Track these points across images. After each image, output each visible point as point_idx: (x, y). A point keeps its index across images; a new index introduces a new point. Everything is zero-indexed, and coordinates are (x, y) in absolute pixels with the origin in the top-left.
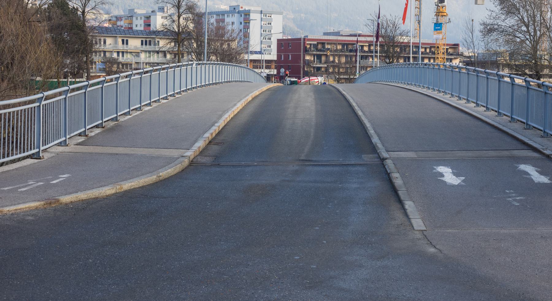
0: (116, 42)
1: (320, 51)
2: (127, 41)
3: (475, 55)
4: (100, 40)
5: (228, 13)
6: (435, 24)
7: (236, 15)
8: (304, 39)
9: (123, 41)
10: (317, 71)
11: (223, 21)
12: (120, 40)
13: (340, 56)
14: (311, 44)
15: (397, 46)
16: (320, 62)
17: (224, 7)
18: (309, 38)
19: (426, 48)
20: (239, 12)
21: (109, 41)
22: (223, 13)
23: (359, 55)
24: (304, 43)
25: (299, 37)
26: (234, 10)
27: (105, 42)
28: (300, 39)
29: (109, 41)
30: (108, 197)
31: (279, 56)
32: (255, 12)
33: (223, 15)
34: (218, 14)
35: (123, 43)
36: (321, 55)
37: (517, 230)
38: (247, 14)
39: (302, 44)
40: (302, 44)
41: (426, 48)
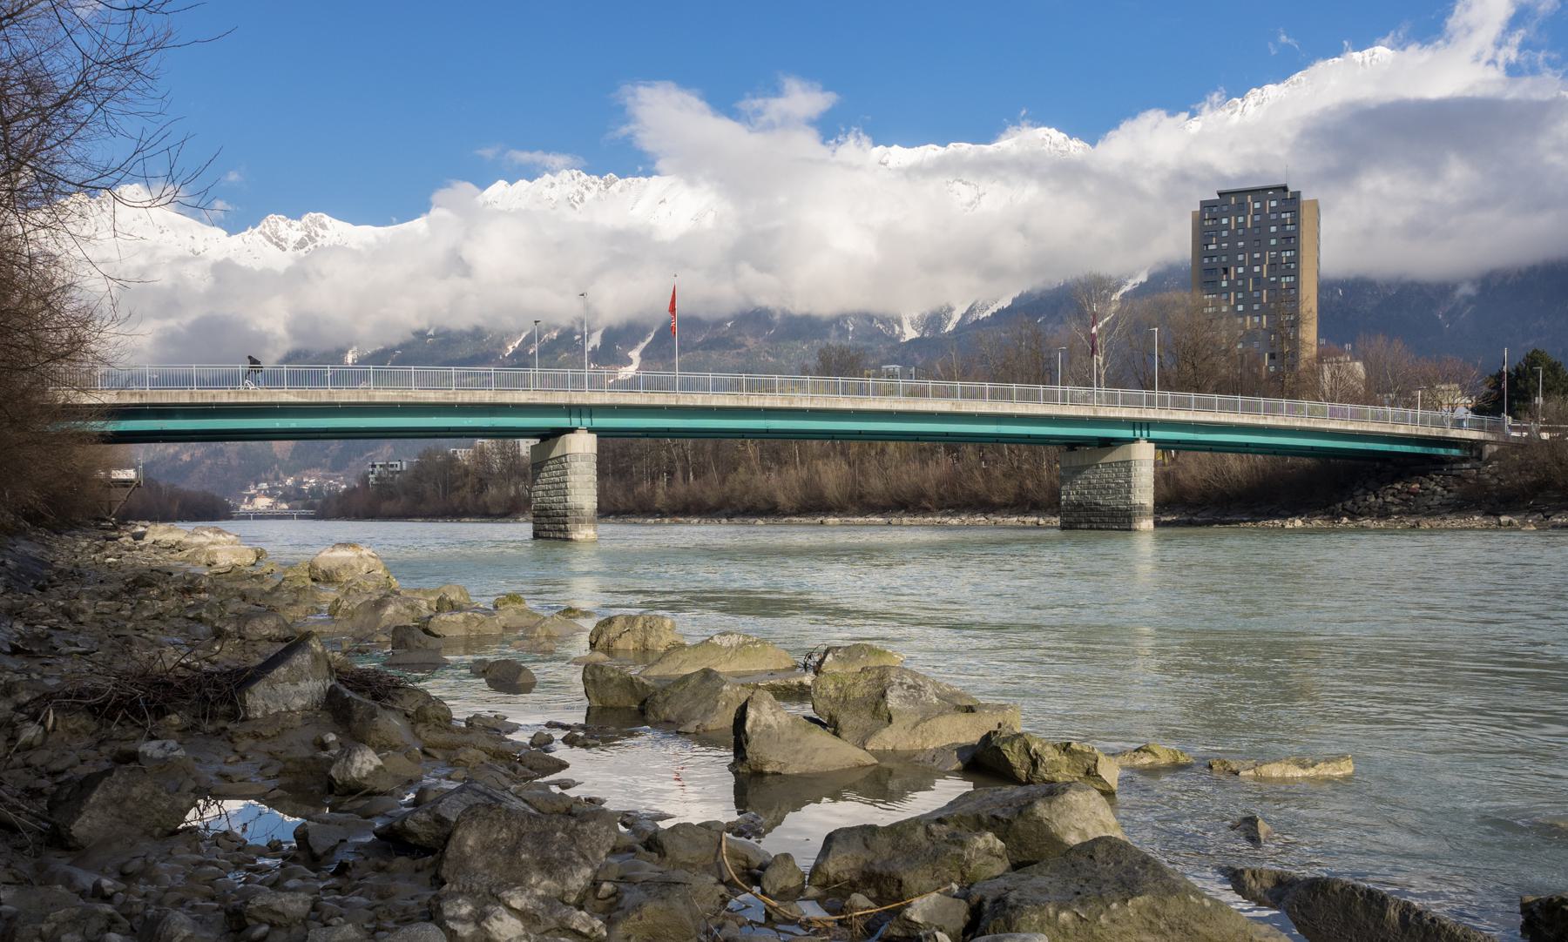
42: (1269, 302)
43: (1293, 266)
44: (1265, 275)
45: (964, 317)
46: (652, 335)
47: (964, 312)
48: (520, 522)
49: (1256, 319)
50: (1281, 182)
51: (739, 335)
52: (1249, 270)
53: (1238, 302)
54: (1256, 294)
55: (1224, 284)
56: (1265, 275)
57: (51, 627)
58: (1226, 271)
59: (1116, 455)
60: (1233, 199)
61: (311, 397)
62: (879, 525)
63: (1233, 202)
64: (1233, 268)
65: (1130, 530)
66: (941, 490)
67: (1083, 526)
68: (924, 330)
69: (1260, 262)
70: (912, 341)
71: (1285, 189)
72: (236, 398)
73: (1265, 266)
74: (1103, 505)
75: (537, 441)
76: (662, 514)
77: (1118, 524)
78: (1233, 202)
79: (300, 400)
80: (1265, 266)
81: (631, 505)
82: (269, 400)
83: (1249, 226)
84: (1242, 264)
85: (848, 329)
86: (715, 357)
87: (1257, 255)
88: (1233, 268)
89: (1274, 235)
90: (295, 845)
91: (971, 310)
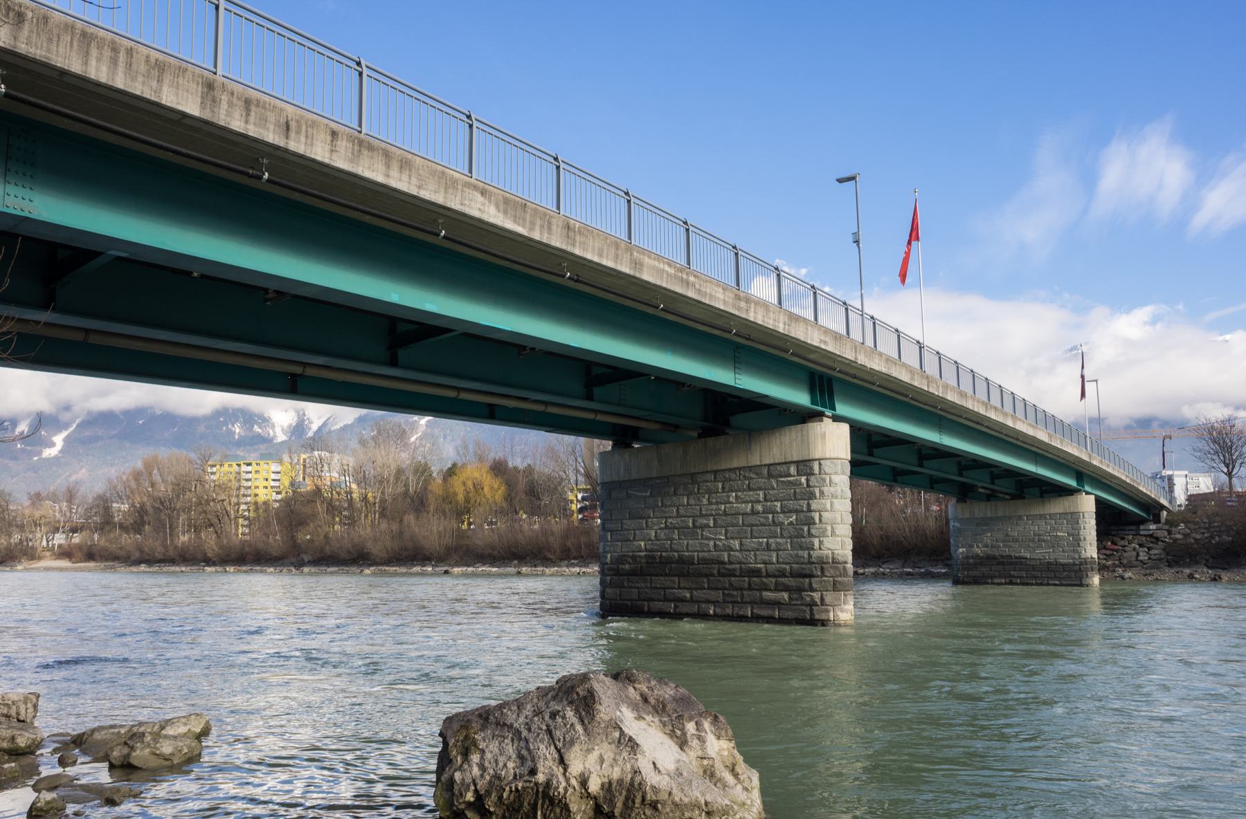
45: (320, 429)
46: (75, 426)
47: (320, 425)
48: (16, 570)
59: (1058, 506)
61: (531, 229)
62: (512, 575)
65: (1081, 585)
66: (569, 544)
67: (996, 581)
68: (291, 436)
70: (282, 442)
72: (355, 157)
74: (1030, 559)
75: (608, 445)
76: (209, 562)
77: (1060, 579)
79: (509, 225)
81: (171, 553)
82: (439, 198)
85: (235, 432)
91: (325, 424)
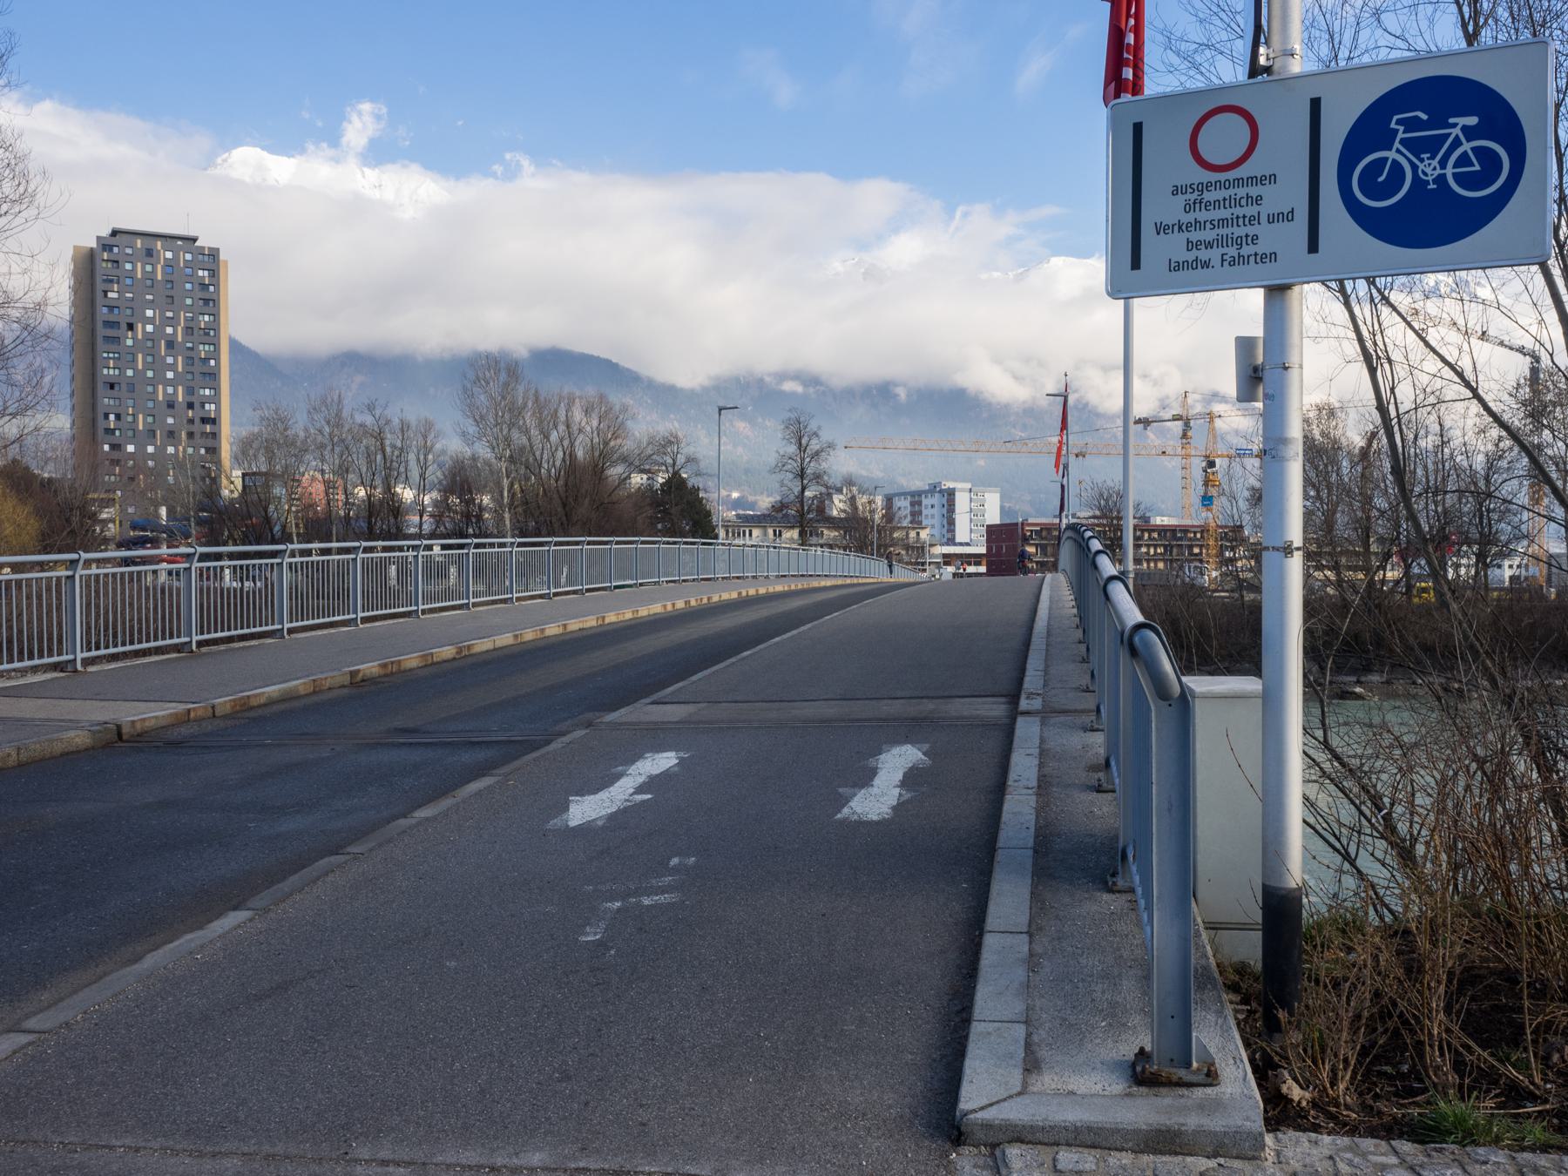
0: (765, 534)
1: (1045, 539)
2: (780, 531)
3: (242, 589)
4: (744, 532)
5: (925, 492)
6: (1203, 497)
7: (936, 495)
8: (1022, 524)
9: (775, 531)
10: (1041, 566)
11: (920, 503)
12: (770, 531)
13: (1155, 546)
14: (1032, 531)
15: (1154, 531)
16: (1046, 555)
17: (919, 484)
18: (1030, 521)
19: (1195, 533)
20: (941, 491)
21: (756, 532)
22: (919, 493)
23: (81, 576)
24: (1023, 529)
25: (1015, 521)
26: (934, 489)
27: (750, 535)
28: (1017, 524)
29: (756, 532)
30: (219, 916)
31: (989, 548)
32: (962, 490)
33: (920, 496)
34: (913, 494)
35: (775, 534)
36: (1046, 545)
37: (1389, 626)
38: (951, 494)
39: (1020, 530)
40: (1020, 530)
41: (1195, 533)
42: (145, 369)
43: (212, 333)
44: (180, 339)
49: (170, 390)
50: (192, 234)
51: (1393, 566)
52: (159, 329)
53: (147, 366)
54: (170, 360)
55: (129, 342)
56: (180, 339)
57: (1219, 1165)
58: (131, 327)
60: (139, 242)
63: (139, 245)
64: (140, 325)
69: (172, 322)
71: (195, 240)
73: (180, 329)
78: (139, 245)
80: (180, 329)
83: (139, 276)
84: (151, 321)
86: (487, 515)
87: (169, 314)
88: (140, 325)
89: (189, 294)
90: (1270, 1072)
